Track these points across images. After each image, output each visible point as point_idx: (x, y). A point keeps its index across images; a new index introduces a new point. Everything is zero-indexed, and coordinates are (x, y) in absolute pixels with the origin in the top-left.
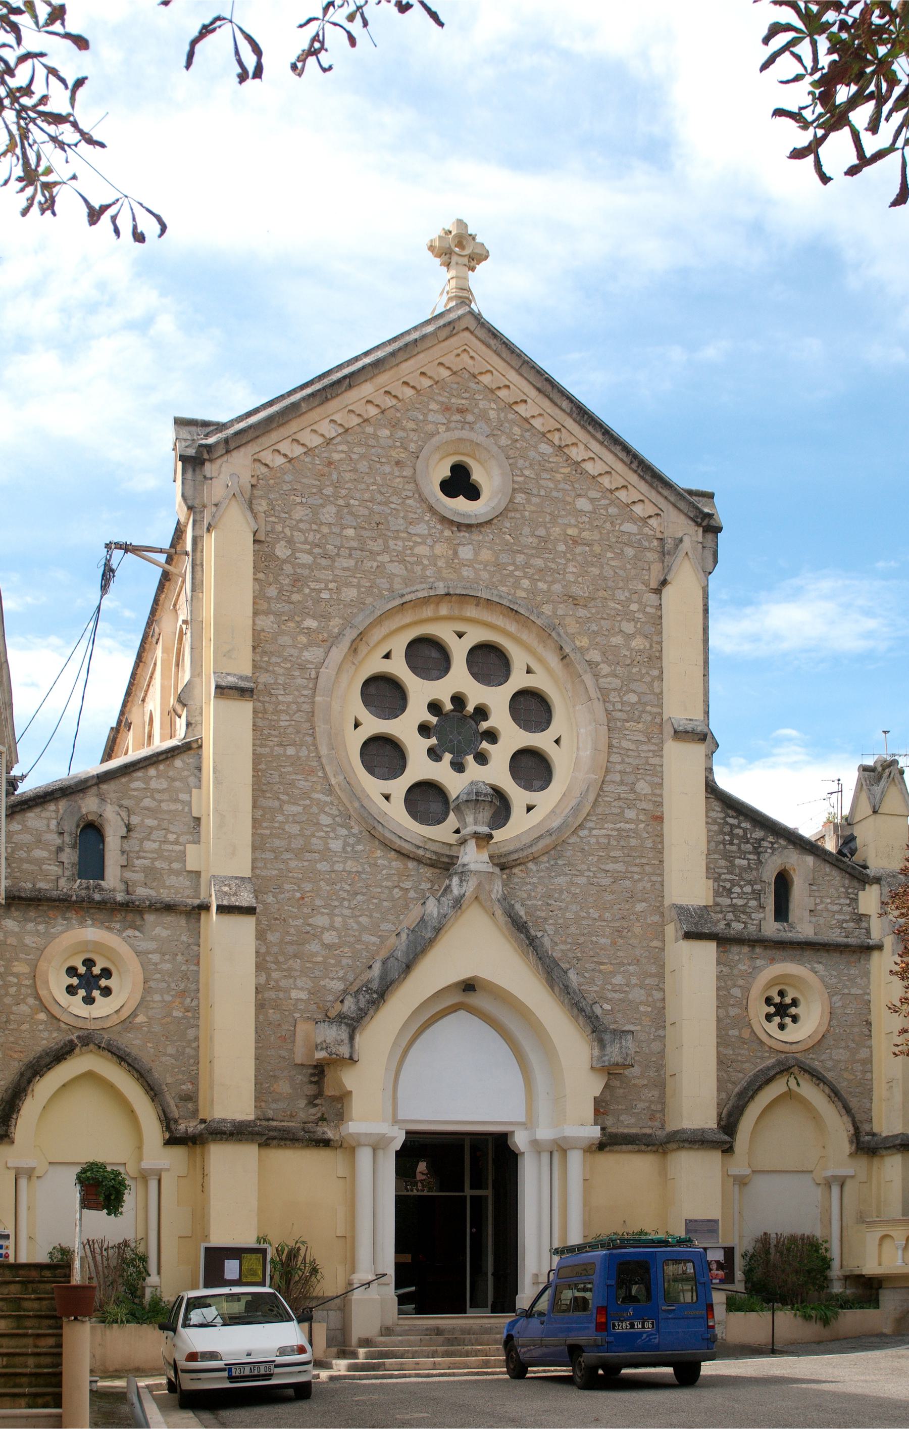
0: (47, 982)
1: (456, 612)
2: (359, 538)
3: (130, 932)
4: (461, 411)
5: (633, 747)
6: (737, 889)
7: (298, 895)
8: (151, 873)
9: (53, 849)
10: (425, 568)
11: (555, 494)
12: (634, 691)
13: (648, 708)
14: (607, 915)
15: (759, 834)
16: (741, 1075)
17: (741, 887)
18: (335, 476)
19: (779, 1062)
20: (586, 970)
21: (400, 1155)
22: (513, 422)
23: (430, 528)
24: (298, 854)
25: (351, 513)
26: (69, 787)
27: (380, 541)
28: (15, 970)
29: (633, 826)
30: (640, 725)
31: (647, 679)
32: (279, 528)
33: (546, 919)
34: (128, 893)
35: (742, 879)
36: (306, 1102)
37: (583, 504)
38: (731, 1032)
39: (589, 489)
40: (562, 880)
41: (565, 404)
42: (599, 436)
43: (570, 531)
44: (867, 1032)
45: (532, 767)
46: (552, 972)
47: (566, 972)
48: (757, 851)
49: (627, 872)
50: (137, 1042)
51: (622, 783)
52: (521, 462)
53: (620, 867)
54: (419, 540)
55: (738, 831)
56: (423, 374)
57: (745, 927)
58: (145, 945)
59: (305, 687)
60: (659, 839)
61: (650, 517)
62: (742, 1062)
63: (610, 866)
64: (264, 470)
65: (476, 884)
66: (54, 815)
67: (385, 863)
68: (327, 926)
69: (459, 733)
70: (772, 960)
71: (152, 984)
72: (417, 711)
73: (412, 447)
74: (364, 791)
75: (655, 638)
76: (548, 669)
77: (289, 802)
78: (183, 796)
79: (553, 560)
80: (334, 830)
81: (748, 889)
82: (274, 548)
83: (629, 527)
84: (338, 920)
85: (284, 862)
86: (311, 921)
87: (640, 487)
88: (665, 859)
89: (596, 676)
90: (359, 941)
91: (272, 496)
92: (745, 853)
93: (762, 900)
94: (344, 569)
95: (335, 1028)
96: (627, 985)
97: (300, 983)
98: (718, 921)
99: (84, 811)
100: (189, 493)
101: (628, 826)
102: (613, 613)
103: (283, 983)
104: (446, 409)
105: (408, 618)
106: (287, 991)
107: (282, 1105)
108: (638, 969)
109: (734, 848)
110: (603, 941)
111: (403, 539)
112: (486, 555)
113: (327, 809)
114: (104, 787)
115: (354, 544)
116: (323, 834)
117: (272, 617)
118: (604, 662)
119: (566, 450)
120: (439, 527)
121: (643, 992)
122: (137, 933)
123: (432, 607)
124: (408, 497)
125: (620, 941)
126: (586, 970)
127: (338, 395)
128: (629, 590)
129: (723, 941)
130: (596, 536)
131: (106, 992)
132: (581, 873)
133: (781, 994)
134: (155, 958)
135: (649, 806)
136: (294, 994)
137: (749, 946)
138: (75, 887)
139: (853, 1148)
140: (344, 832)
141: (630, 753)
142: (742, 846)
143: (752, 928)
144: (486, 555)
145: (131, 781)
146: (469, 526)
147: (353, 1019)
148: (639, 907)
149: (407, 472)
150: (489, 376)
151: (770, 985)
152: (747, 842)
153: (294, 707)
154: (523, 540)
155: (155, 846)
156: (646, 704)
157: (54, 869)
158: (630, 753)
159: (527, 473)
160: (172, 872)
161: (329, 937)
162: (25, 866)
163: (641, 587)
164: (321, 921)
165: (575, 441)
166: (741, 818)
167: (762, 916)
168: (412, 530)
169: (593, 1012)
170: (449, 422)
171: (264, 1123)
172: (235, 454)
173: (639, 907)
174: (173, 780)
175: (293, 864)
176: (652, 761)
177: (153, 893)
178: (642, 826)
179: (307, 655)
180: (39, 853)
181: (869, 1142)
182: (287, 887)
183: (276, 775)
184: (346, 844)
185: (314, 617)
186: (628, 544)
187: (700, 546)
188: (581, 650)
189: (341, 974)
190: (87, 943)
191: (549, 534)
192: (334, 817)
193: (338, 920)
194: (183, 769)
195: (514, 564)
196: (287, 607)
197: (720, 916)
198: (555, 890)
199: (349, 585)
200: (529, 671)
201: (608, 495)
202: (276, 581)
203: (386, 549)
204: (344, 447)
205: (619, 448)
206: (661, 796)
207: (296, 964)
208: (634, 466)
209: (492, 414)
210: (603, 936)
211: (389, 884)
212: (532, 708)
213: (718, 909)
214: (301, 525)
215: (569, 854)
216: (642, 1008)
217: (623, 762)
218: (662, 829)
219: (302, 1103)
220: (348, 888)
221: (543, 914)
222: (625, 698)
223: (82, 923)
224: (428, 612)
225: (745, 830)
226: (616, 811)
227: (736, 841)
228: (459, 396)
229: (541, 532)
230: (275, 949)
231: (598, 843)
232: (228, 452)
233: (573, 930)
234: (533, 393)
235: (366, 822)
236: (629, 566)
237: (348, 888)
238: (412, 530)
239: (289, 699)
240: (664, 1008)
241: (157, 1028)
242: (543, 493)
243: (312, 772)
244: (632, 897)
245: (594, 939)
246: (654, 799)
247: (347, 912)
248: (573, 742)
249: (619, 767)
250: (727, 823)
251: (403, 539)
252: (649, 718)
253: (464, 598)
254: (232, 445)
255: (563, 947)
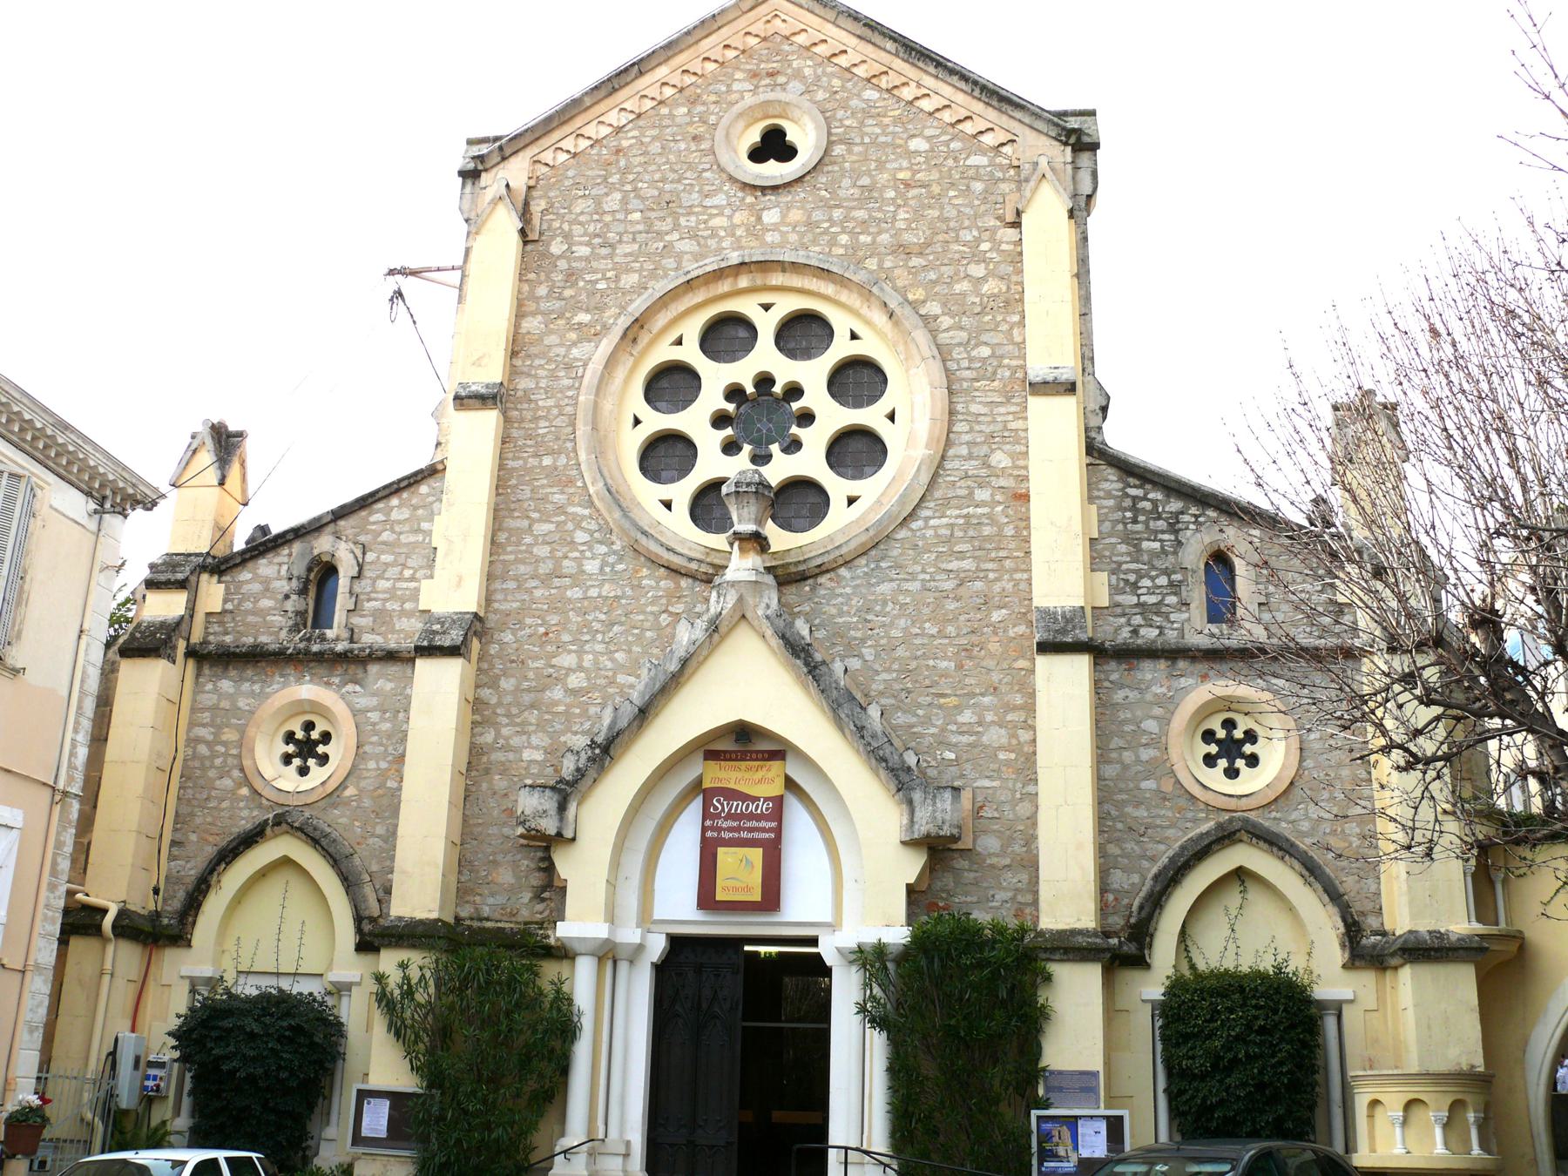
0: (252, 751)
1: (759, 282)
2: (648, 222)
3: (350, 687)
4: (771, 75)
5: (983, 410)
6: (1146, 582)
7: (542, 630)
8: (382, 616)
9: (280, 597)
10: (721, 239)
11: (882, 139)
12: (986, 344)
13: (1006, 361)
14: (951, 630)
15: (1175, 505)
16: (1162, 847)
17: (1153, 579)
18: (622, 163)
19: (1220, 826)
20: (919, 706)
21: (660, 969)
22: (833, 75)
23: (729, 197)
24: (546, 580)
25: (638, 197)
26: (303, 526)
27: (669, 220)
28: (224, 738)
29: (986, 510)
30: (996, 383)
31: (1005, 327)
32: (556, 224)
33: (863, 640)
34: (352, 641)
35: (1153, 568)
36: (530, 895)
37: (917, 144)
38: (1146, 785)
39: (924, 127)
40: (885, 588)
41: (890, 45)
42: (931, 69)
43: (901, 175)
44: (1364, 775)
45: (857, 450)
46: (843, 706)
47: (864, 709)
48: (1174, 528)
49: (978, 569)
50: (343, 820)
51: (970, 457)
52: (840, 114)
53: (967, 564)
54: (715, 211)
55: (1147, 505)
56: (727, 46)
57: (1161, 634)
58: (363, 702)
59: (569, 388)
60: (1024, 524)
61: (1003, 144)
62: (1162, 827)
63: (954, 565)
64: (545, 169)
65: (735, 598)
66: (286, 559)
67: (653, 583)
68: (574, 666)
69: (770, 421)
70: (1205, 677)
71: (367, 748)
72: (816, 397)
73: (712, 119)
74: (633, 499)
75: (1014, 278)
76: (880, 333)
77: (540, 521)
78: (425, 526)
79: (880, 209)
80: (591, 549)
81: (1163, 581)
82: (549, 244)
83: (975, 160)
84: (588, 660)
85: (529, 591)
86: (554, 661)
87: (985, 115)
88: (1033, 549)
89: (934, 333)
90: (612, 683)
91: (552, 194)
92: (1156, 532)
93: (1184, 594)
94: (626, 255)
95: (536, 795)
96: (980, 723)
97: (535, 740)
98: (1120, 627)
99: (316, 552)
100: (466, 207)
101: (979, 510)
102: (957, 256)
103: (516, 741)
104: (755, 75)
105: (699, 296)
106: (517, 750)
107: (500, 899)
108: (995, 700)
109: (1139, 527)
110: (944, 664)
111: (697, 214)
112: (796, 215)
113: (584, 524)
114: (342, 523)
115: (640, 227)
116: (577, 554)
117: (540, 318)
118: (944, 314)
119: (895, 92)
120: (740, 194)
121: (1003, 731)
122: (358, 688)
123: (730, 280)
124: (704, 170)
125: (969, 664)
126: (919, 706)
127: (627, 84)
128: (978, 228)
129: (1098, 652)
130: (935, 175)
131: (1253, 761)
132: (912, 577)
133: (1229, 724)
134: (374, 716)
135: (1008, 482)
136: (527, 755)
137: (1167, 658)
138: (294, 643)
139: (1347, 955)
140: (603, 549)
141: (981, 419)
142: (1152, 524)
143: (1171, 635)
144: (796, 215)
145: (370, 514)
146: (775, 188)
147: (567, 783)
148: (996, 616)
149: (705, 145)
150: (803, 35)
151: (1206, 710)
152: (1159, 518)
153: (555, 411)
154: (842, 193)
155: (388, 584)
156: (1002, 357)
157: (277, 619)
158: (981, 419)
159: (847, 123)
160: (403, 613)
161: (575, 681)
162: (250, 619)
163: (993, 222)
164: (568, 660)
165: (904, 80)
166: (1148, 486)
167: (1186, 616)
168: (708, 202)
169: (903, 762)
170: (757, 87)
171: (476, 924)
172: (513, 160)
173: (996, 616)
174: (416, 508)
175: (538, 593)
176: (1012, 425)
177: (379, 639)
178: (999, 508)
179: (575, 352)
180: (266, 603)
181: (1374, 946)
182: (528, 621)
183: (527, 489)
184: (604, 564)
185: (587, 311)
186: (976, 178)
187: (1069, 167)
188: (914, 305)
189: (587, 726)
190: (301, 702)
191: (874, 183)
192: (591, 533)
193: (588, 660)
194: (428, 495)
195: (830, 220)
196: (558, 304)
197: (1123, 620)
198: (876, 601)
199: (629, 271)
200: (854, 336)
201: (951, 130)
202: (548, 278)
203: (676, 227)
204: (635, 133)
205: (955, 78)
206: (1026, 468)
207: (533, 717)
208: (977, 93)
209: (807, 72)
210: (945, 658)
211: (655, 609)
212: (858, 379)
213: (1119, 610)
214: (582, 218)
215: (895, 553)
216: (1002, 756)
217: (971, 430)
218: (1028, 510)
219: (527, 896)
220: (603, 617)
221: (859, 634)
222: (974, 353)
223: (299, 680)
224: (725, 286)
225: (1154, 502)
226: (964, 492)
227: (1141, 518)
228: (768, 61)
229: (865, 181)
230: (508, 699)
231: (937, 535)
232: (504, 159)
233: (900, 652)
234: (854, 41)
235: (628, 536)
236: (977, 202)
237: (603, 617)
238: (708, 202)
239: (550, 402)
240: (1034, 753)
241: (367, 803)
242: (867, 140)
243: (571, 482)
244: (986, 602)
245: (931, 663)
246: (1016, 473)
247: (600, 648)
248: (908, 414)
249: (966, 438)
250: (1127, 495)
251: (697, 214)
252: (1007, 374)
253: (765, 266)
254: (508, 152)
255: (885, 676)
